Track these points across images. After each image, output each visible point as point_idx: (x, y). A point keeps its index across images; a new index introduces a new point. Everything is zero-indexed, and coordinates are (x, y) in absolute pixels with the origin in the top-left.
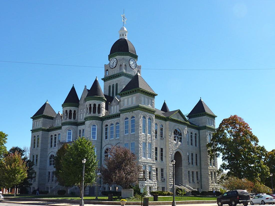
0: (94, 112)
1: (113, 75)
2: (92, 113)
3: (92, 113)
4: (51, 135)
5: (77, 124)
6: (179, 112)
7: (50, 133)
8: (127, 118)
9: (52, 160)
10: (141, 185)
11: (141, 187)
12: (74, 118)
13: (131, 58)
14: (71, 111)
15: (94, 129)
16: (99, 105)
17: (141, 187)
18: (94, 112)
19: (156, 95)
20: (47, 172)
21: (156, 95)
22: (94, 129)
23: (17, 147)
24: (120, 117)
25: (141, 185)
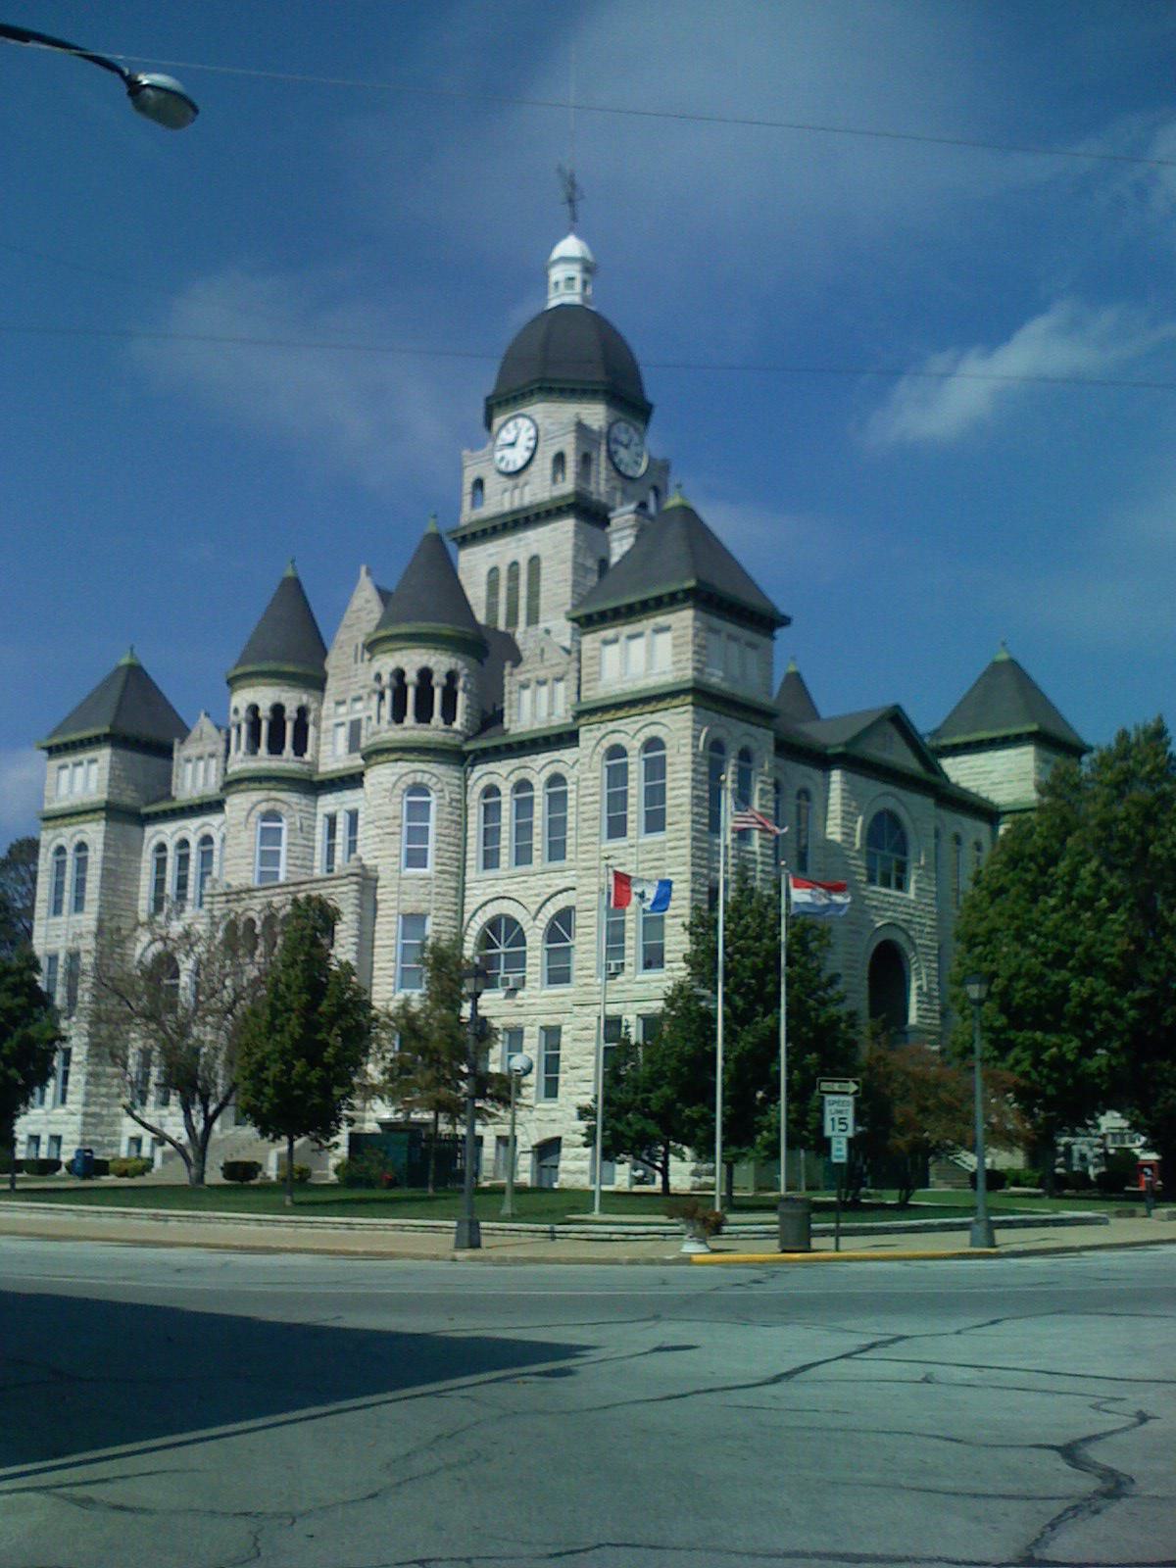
0: (276, 748)
1: (513, 512)
2: (263, 749)
3: (263, 749)
4: (154, 842)
5: (314, 786)
6: (897, 719)
7: (150, 830)
8: (616, 751)
9: (502, 949)
10: (833, 1119)
11: (836, 1133)
12: (300, 747)
13: (622, 416)
14: (425, 674)
15: (418, 811)
16: (302, 712)
17: (836, 1133)
18: (276, 748)
19: (785, 621)
20: (536, 1029)
21: (785, 621)
22: (418, 811)
23: (1124, 735)
24: (577, 746)
25: (833, 1119)
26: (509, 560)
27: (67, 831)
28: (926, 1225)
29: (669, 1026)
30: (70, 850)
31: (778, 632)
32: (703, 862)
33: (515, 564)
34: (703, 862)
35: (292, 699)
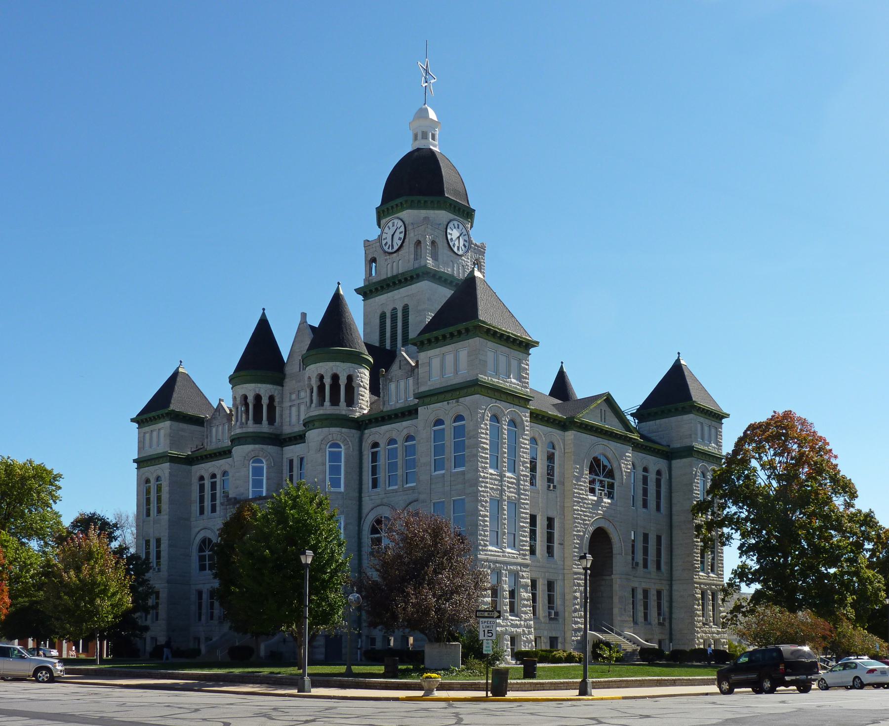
1: (393, 277)
2: (327, 403)
3: (327, 403)
4: (198, 475)
5: (280, 440)
11: (486, 638)
12: (271, 420)
16: (271, 398)
17: (486, 638)
19: (535, 344)
26: (390, 307)
27: (152, 468)
28: (551, 683)
29: (744, 550)
30: (152, 481)
31: (532, 351)
32: (496, 483)
33: (395, 309)
34: (496, 483)
35: (265, 390)
